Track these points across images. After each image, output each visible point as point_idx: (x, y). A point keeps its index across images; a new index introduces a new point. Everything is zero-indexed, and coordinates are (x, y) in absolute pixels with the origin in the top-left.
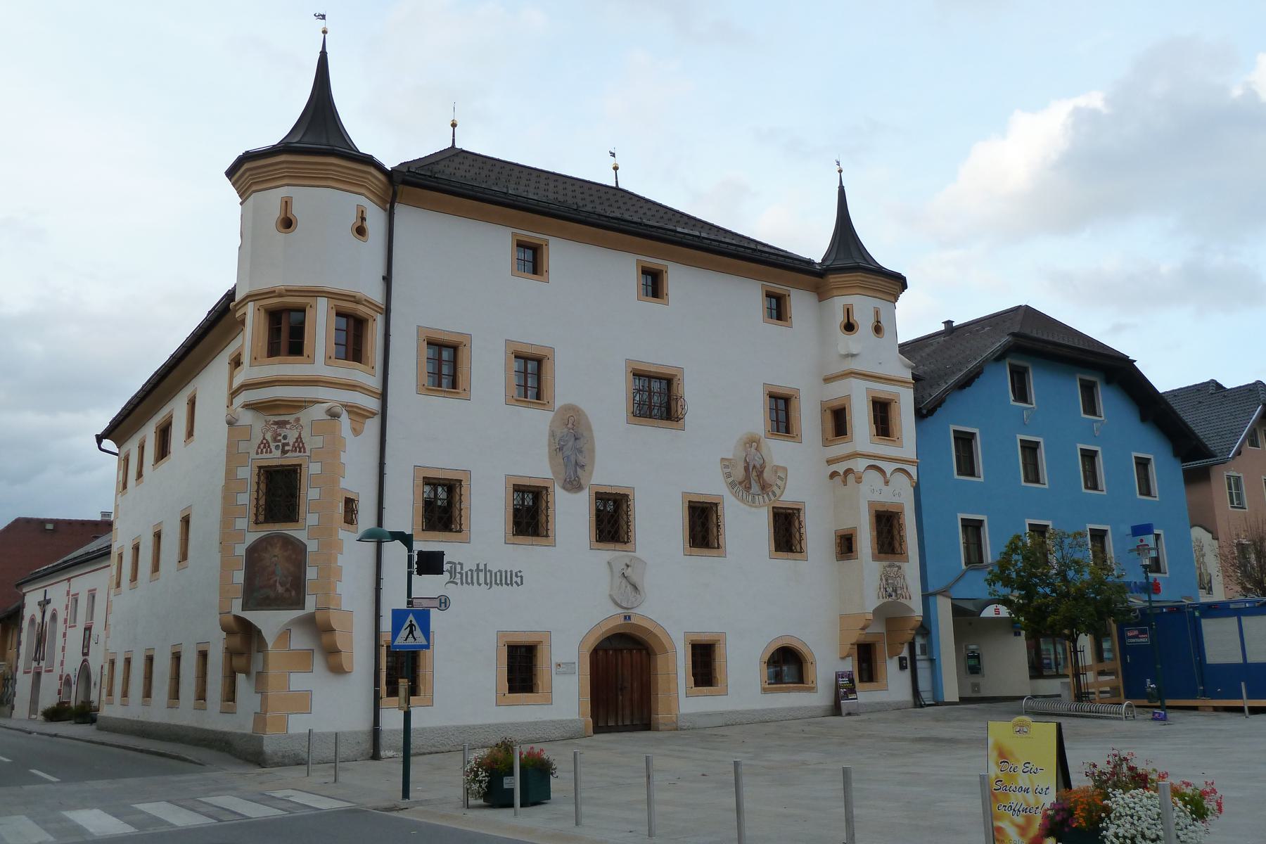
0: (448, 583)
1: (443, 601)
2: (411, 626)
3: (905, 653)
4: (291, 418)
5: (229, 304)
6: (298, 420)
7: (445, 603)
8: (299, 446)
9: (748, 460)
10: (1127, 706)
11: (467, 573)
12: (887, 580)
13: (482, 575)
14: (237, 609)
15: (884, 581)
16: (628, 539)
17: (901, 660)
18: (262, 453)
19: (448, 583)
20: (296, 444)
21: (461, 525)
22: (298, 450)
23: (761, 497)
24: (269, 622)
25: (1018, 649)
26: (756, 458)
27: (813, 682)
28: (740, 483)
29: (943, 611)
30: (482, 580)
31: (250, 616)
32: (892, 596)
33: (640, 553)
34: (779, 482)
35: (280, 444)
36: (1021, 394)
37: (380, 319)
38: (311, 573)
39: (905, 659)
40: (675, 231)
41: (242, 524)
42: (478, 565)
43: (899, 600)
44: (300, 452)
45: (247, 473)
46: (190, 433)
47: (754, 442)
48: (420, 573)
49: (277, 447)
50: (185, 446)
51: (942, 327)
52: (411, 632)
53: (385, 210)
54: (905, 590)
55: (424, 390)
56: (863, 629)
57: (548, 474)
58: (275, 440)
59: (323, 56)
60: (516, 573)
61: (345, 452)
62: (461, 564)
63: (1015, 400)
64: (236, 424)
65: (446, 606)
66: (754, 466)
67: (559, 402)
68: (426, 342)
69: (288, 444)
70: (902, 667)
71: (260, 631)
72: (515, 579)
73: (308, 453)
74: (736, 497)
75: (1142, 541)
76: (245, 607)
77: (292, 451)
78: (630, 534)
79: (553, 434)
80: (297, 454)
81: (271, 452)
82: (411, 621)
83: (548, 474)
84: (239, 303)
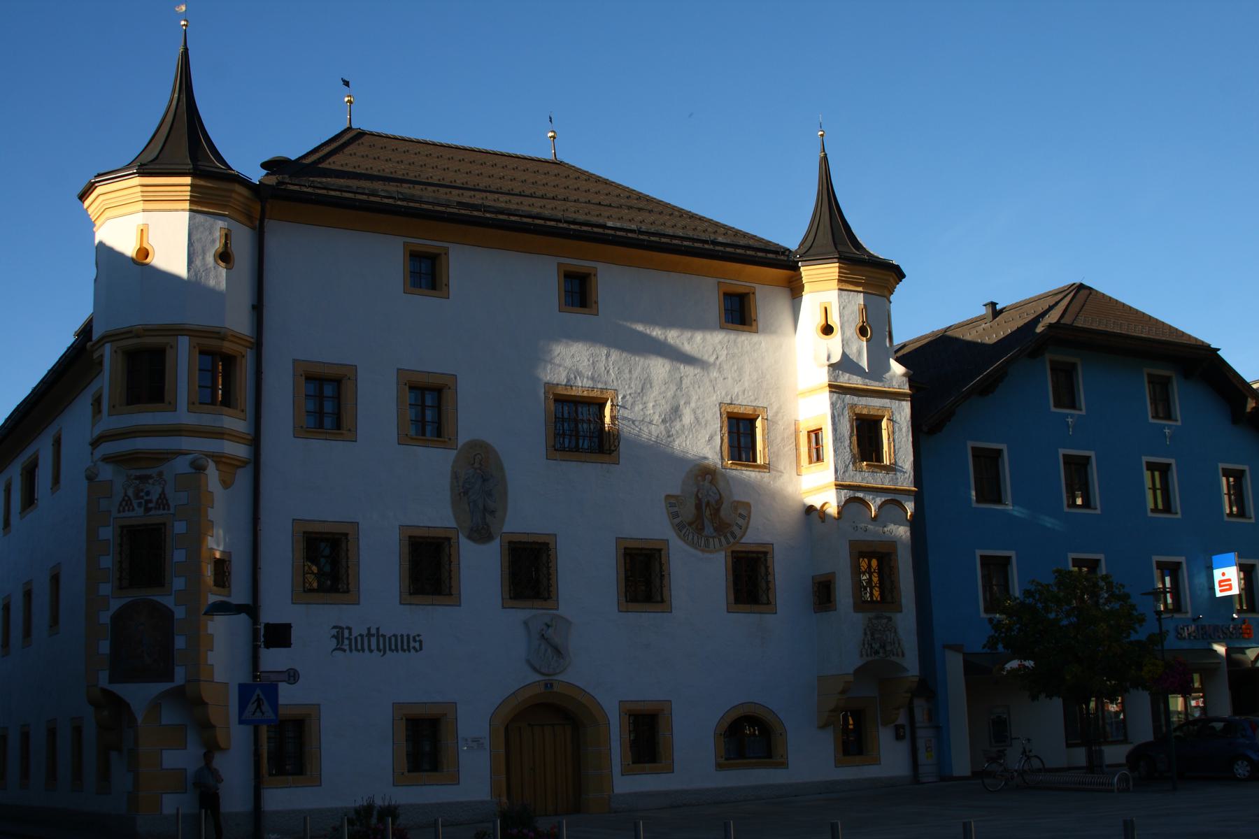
0: (334, 650)
1: (292, 674)
2: (259, 700)
3: (902, 719)
4: (153, 472)
5: (86, 343)
6: (160, 474)
7: (294, 676)
8: (163, 502)
9: (700, 496)
10: (1119, 779)
11: (356, 638)
12: (872, 635)
13: (374, 640)
14: (103, 679)
15: (869, 637)
16: (549, 594)
17: (897, 728)
18: (124, 511)
19: (334, 650)
20: (160, 501)
21: (348, 584)
22: (162, 506)
23: (716, 540)
24: (139, 695)
25: (1052, 712)
26: (711, 493)
27: (782, 756)
28: (690, 524)
29: (954, 666)
30: (374, 646)
31: (118, 689)
32: (879, 653)
33: (563, 610)
34: (740, 521)
35: (143, 501)
36: (1066, 397)
37: (249, 355)
38: (180, 643)
39: (903, 726)
40: (604, 227)
41: (105, 589)
42: (369, 629)
43: (888, 658)
44: (164, 509)
45: (107, 533)
46: (56, 480)
47: (707, 474)
48: (267, 646)
49: (140, 505)
50: (53, 494)
51: (983, 311)
52: (259, 706)
53: (253, 228)
54: (897, 645)
55: (301, 431)
56: (843, 692)
57: (452, 523)
58: (137, 496)
60: (414, 638)
61: (213, 508)
62: (350, 629)
63: (1055, 406)
64: (97, 480)
65: (294, 680)
67: (463, 439)
68: (303, 378)
69: (151, 501)
70: (899, 737)
71: (128, 705)
72: (412, 644)
73: (172, 511)
74: (684, 541)
75: (1223, 574)
76: (112, 680)
77: (156, 508)
78: (551, 589)
79: (455, 476)
80: (161, 512)
81: (133, 510)
82: (258, 695)
83: (452, 523)
84: (98, 341)
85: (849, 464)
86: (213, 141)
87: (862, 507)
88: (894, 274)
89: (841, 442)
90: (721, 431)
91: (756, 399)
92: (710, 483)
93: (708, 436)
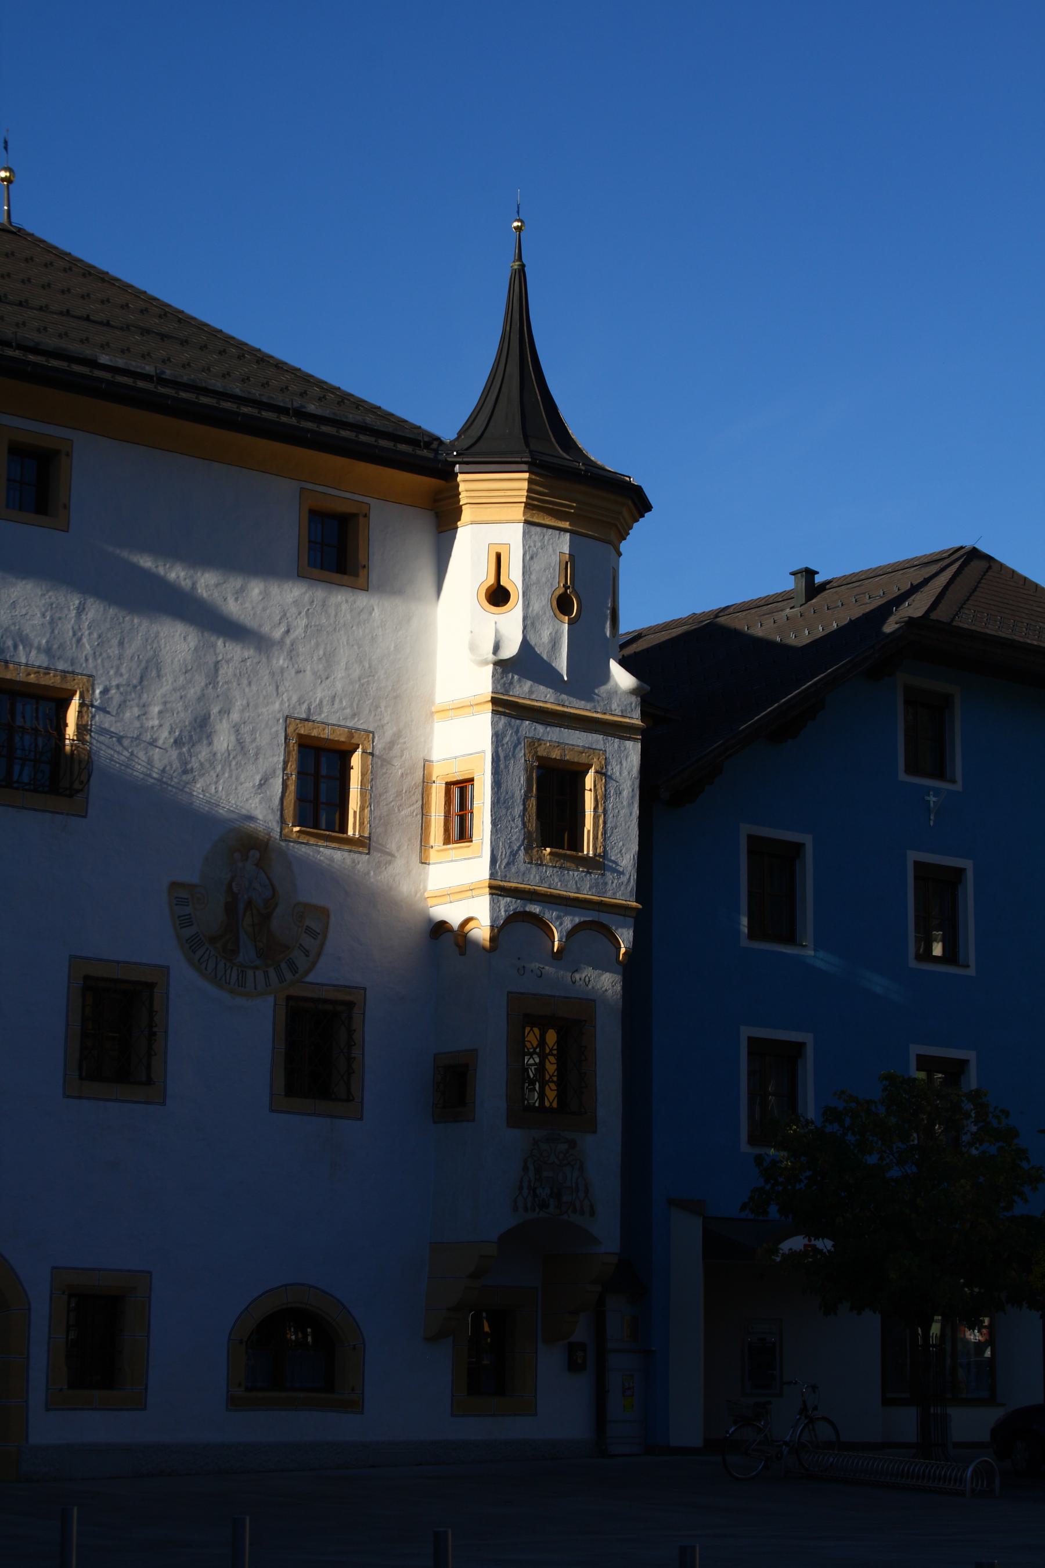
9: (235, 890)
51: (789, 584)
59: (520, 276)
66: (249, 903)
90: (284, 769)
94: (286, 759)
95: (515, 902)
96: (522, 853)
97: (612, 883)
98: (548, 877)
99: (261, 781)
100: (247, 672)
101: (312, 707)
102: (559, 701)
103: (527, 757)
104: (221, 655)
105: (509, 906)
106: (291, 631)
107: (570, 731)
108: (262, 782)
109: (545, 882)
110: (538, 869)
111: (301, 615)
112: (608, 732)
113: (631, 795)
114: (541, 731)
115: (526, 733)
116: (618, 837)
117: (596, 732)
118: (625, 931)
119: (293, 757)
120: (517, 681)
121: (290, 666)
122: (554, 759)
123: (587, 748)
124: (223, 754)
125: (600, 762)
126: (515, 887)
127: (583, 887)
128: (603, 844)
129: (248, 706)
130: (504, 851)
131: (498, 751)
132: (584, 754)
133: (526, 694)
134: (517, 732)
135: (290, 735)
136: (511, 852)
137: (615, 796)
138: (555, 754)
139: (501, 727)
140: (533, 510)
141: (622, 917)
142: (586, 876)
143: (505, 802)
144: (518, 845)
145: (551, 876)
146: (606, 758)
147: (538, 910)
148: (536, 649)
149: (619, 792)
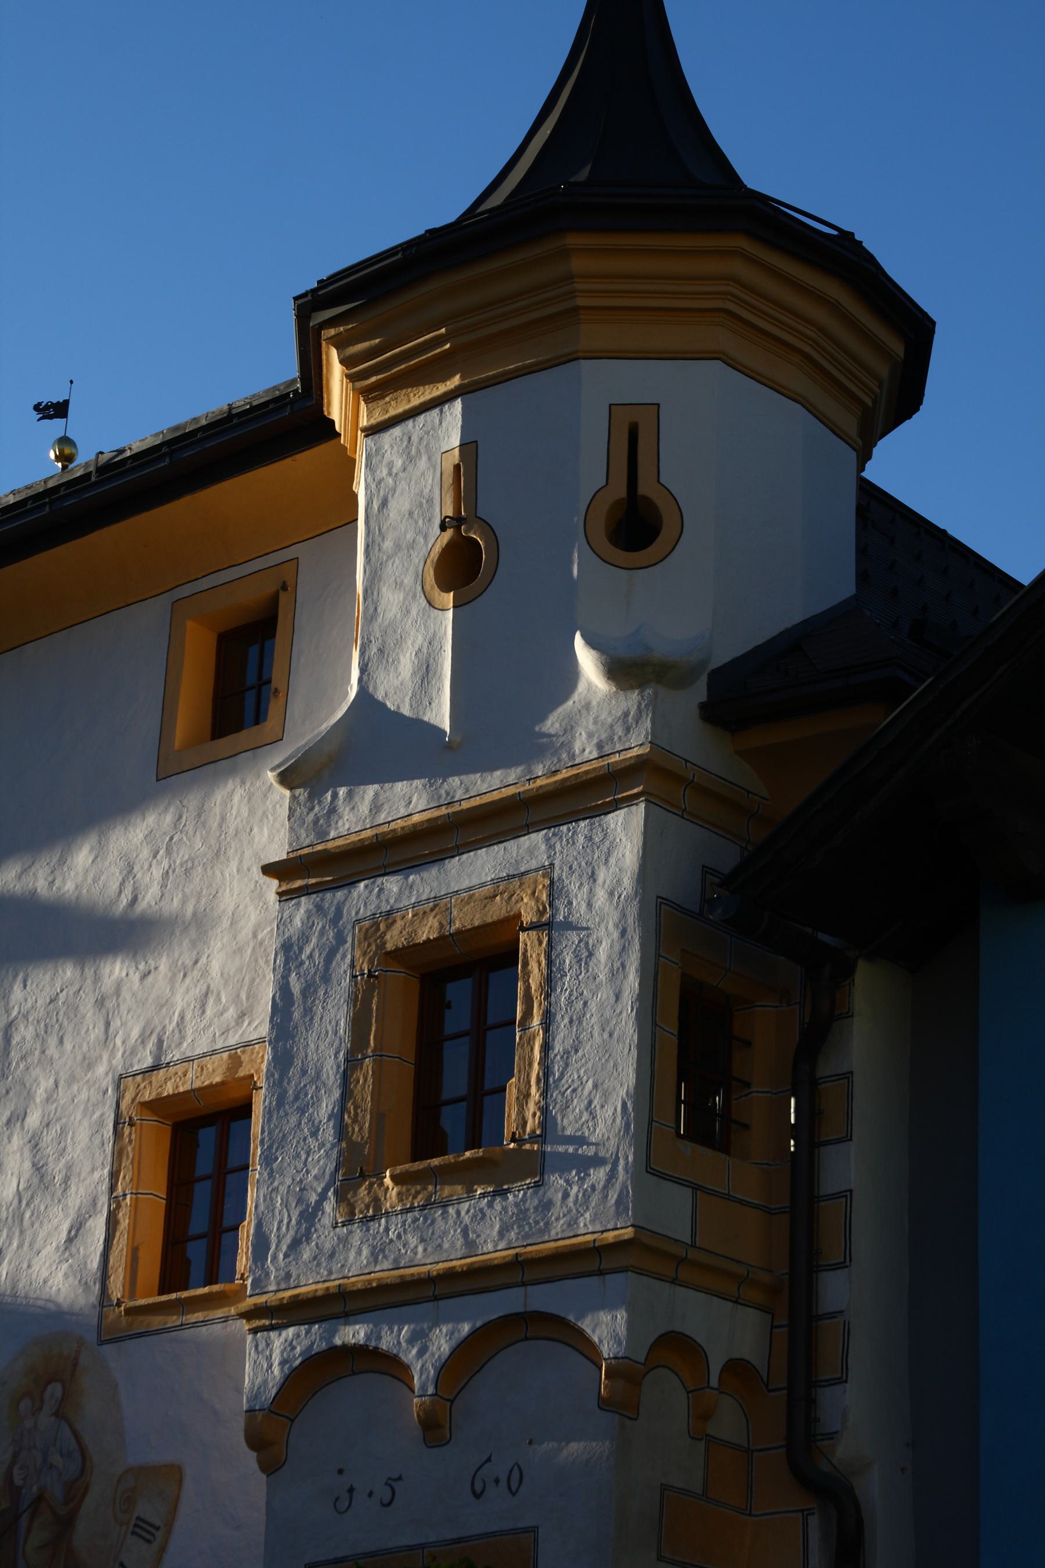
9: (18, 1480)
85: (323, 1196)
86: (887, 436)
87: (411, 1392)
88: (572, 240)
89: (302, 1111)
90: (112, 1188)
91: (242, 1015)
92: (56, 1414)
93: (65, 1227)
94: (115, 1168)
95: (308, 1332)
96: (329, 1207)
97: (566, 1195)
98: (391, 1241)
99: (70, 1232)
100: (57, 1020)
101: (165, 1038)
102: (440, 797)
103: (358, 968)
104: (16, 1009)
105: (294, 1348)
106: (140, 897)
107: (465, 856)
108: (73, 1233)
109: (385, 1257)
110: (368, 1230)
111: (158, 857)
112: (686, 794)
113: (617, 947)
114: (395, 889)
115: (357, 913)
116: (583, 1070)
117: (528, 829)
118: (605, 1317)
119: (128, 1157)
120: (345, 800)
121: (131, 972)
122: (425, 942)
123: (503, 879)
124: (11, 1205)
125: (538, 900)
126: (290, 1297)
127: (483, 1237)
128: (542, 1103)
129: (57, 1086)
130: (286, 1216)
131: (288, 983)
132: (498, 898)
133: (364, 821)
134: (335, 921)
135: (125, 1113)
136: (301, 1214)
137: (576, 967)
138: (427, 931)
139: (299, 924)
140: (383, 397)
141: (594, 1281)
142: (490, 1205)
143: (297, 1098)
144: (319, 1190)
145: (399, 1237)
146: (552, 883)
147: (362, 1334)
148: (389, 705)
149: (585, 954)
